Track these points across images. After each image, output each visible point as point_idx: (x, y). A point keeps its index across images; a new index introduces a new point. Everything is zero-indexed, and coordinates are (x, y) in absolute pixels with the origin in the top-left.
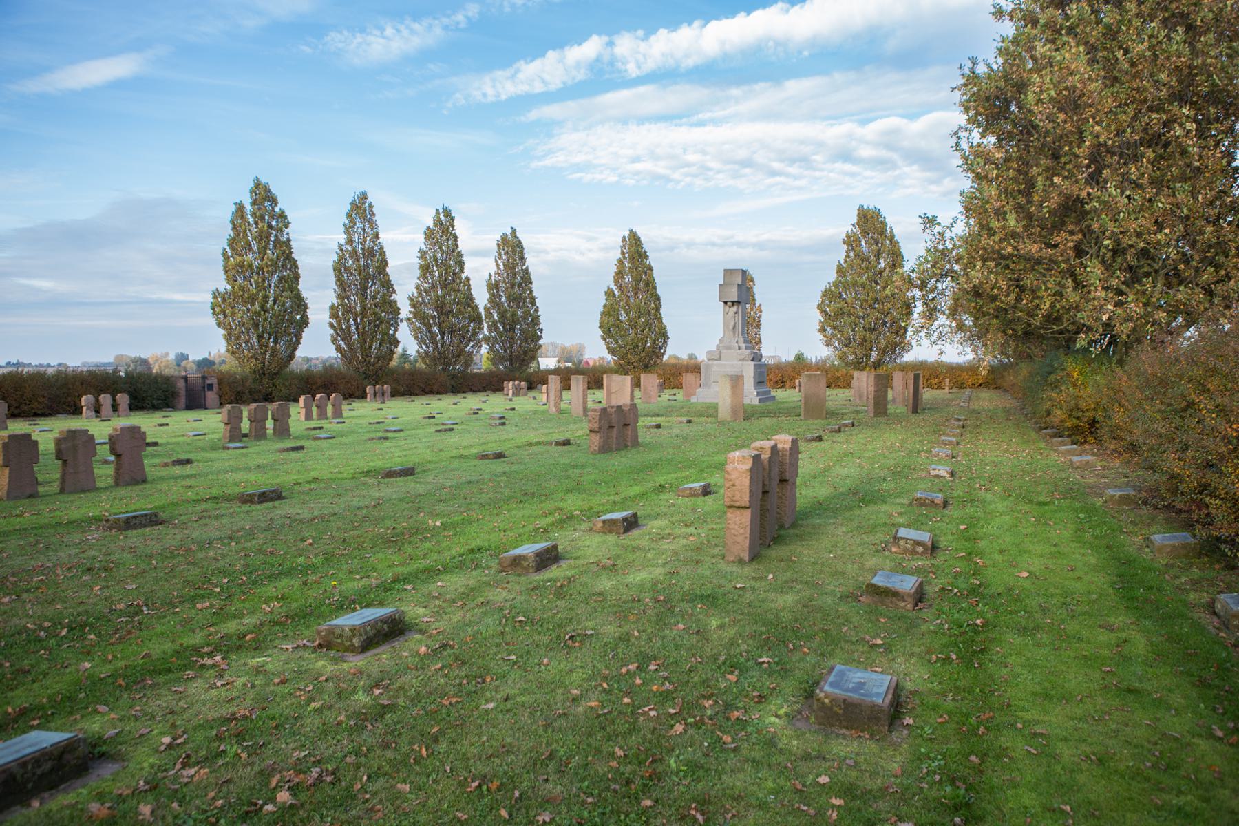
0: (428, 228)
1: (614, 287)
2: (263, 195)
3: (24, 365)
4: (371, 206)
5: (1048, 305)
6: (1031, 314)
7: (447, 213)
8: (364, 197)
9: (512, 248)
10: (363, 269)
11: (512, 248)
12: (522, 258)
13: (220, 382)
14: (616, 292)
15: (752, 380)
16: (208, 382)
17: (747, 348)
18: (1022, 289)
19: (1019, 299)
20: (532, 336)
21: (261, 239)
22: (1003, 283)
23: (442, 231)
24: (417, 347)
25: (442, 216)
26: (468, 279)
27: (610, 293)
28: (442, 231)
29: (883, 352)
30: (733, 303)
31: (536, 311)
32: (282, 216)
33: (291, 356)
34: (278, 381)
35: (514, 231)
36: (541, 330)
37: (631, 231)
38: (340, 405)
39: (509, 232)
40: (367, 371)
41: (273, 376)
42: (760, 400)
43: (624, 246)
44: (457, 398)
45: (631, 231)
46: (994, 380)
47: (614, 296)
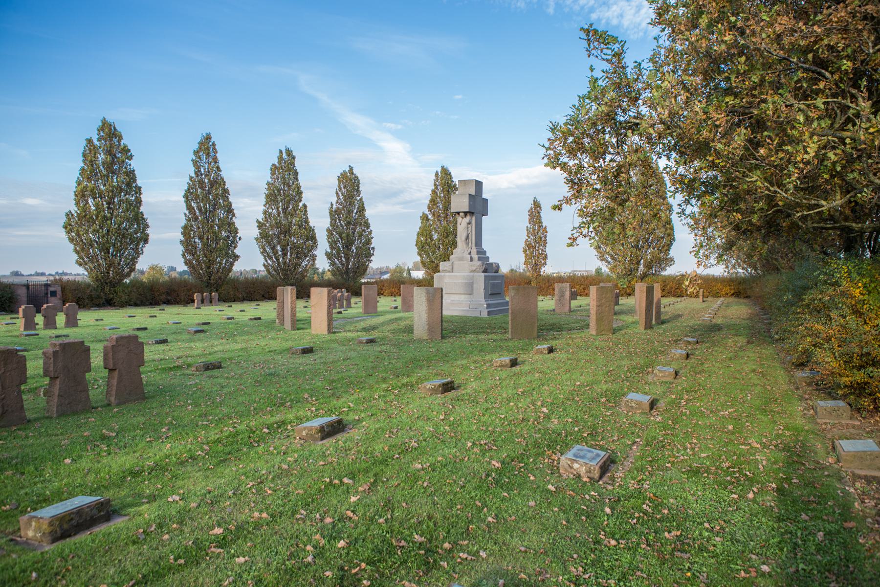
0: (273, 165)
1: (427, 212)
2: (110, 132)
3: (66, 274)
4: (214, 144)
5: (812, 150)
6: (776, 178)
7: (289, 152)
8: (208, 137)
9: (350, 184)
10: (208, 197)
11: (350, 184)
12: (358, 191)
13: (63, 289)
14: (430, 217)
15: (482, 291)
16: (52, 289)
17: (479, 259)
18: (759, 125)
19: (754, 144)
20: (367, 252)
21: (109, 170)
22: (720, 118)
23: (286, 169)
24: (263, 261)
25: (285, 156)
26: (305, 206)
27: (425, 218)
28: (286, 169)
29: (649, 266)
30: (466, 213)
31: (370, 233)
32: (126, 151)
33: (230, 270)
34: (118, 289)
35: (351, 169)
36: (373, 248)
37: (443, 167)
38: (76, 314)
39: (347, 169)
40: (210, 279)
41: (113, 285)
42: (489, 313)
43: (437, 180)
44: (155, 311)
45: (443, 167)
46: (739, 289)
47: (428, 219)
